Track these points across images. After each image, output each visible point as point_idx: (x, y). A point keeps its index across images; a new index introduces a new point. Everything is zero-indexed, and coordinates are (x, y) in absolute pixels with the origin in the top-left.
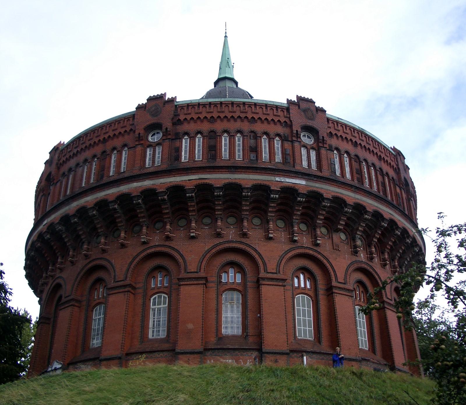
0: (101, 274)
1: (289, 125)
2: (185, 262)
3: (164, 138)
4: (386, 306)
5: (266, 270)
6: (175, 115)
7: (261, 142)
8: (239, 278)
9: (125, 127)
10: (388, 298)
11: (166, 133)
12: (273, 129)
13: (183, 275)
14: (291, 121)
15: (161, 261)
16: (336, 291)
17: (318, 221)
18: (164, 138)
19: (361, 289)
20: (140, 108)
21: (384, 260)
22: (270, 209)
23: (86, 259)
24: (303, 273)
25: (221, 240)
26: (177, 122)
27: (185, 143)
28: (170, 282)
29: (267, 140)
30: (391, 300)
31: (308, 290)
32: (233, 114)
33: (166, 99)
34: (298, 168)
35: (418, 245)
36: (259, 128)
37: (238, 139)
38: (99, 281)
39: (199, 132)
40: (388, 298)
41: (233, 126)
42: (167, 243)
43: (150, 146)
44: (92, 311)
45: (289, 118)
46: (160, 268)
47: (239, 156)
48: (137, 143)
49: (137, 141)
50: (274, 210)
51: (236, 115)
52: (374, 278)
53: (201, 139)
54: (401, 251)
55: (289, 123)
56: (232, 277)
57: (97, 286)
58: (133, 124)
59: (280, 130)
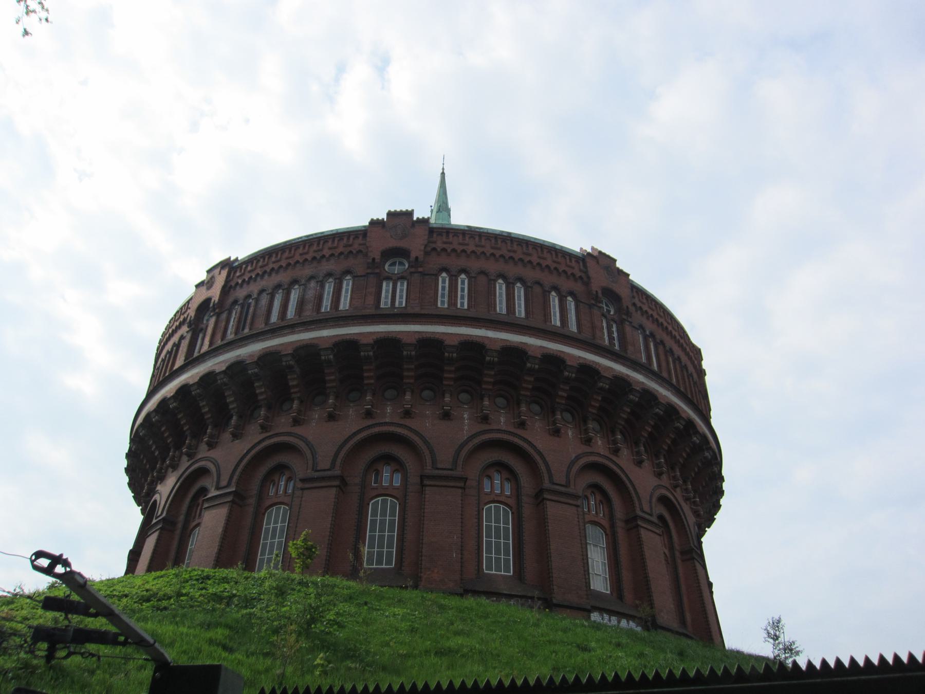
0: (283, 458)
1: (587, 282)
2: (308, 443)
3: (413, 270)
4: (640, 523)
5: (434, 462)
6: (429, 242)
7: (495, 288)
8: (397, 481)
9: (350, 246)
10: (644, 512)
11: (416, 263)
12: (566, 285)
13: (429, 470)
14: (589, 277)
15: (383, 448)
16: (549, 497)
17: (590, 410)
18: (413, 270)
19: (599, 497)
20: (373, 223)
21: (659, 465)
22: (524, 385)
23: (262, 433)
24: (498, 471)
25: (486, 427)
26: (430, 251)
27: (443, 281)
28: (405, 479)
29: (504, 287)
30: (651, 515)
31: (507, 497)
32: (541, 261)
33: (415, 219)
34: (599, 342)
35: (710, 448)
36: (492, 267)
37: (519, 292)
38: (282, 468)
39: (464, 271)
40: (644, 512)
41: (513, 270)
42: (520, 432)
43: (388, 278)
44: (264, 514)
45: (586, 272)
46: (388, 459)
47: (463, 302)
48: (369, 271)
49: (368, 268)
50: (492, 380)
51: (544, 263)
52: (623, 482)
53: (447, 280)
54: (684, 455)
55: (585, 279)
56: (498, 484)
57: (276, 478)
58: (364, 244)
59: (578, 287)
